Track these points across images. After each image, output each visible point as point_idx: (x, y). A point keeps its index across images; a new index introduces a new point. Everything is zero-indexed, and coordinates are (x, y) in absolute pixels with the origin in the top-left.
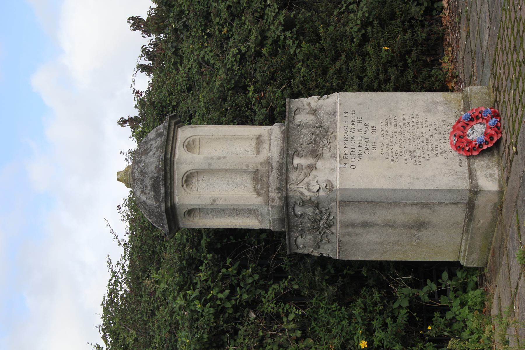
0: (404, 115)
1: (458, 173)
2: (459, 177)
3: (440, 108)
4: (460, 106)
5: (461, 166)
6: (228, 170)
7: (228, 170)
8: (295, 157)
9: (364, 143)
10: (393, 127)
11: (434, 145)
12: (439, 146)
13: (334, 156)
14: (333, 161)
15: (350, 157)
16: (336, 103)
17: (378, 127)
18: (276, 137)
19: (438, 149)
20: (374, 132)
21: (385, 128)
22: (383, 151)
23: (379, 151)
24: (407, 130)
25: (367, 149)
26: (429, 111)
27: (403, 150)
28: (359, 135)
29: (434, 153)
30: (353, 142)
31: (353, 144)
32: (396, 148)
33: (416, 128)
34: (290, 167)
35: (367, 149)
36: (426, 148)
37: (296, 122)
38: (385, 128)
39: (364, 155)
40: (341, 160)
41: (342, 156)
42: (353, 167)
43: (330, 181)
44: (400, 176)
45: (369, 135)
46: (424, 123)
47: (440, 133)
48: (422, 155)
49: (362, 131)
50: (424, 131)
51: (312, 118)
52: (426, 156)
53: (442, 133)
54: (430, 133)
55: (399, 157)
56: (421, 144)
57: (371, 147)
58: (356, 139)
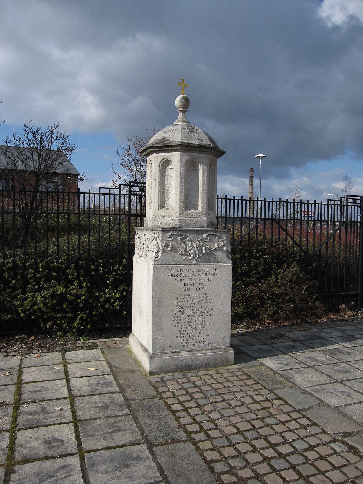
6: (235, 331)
7: (235, 331)
42: (170, 275)
47: (196, 333)
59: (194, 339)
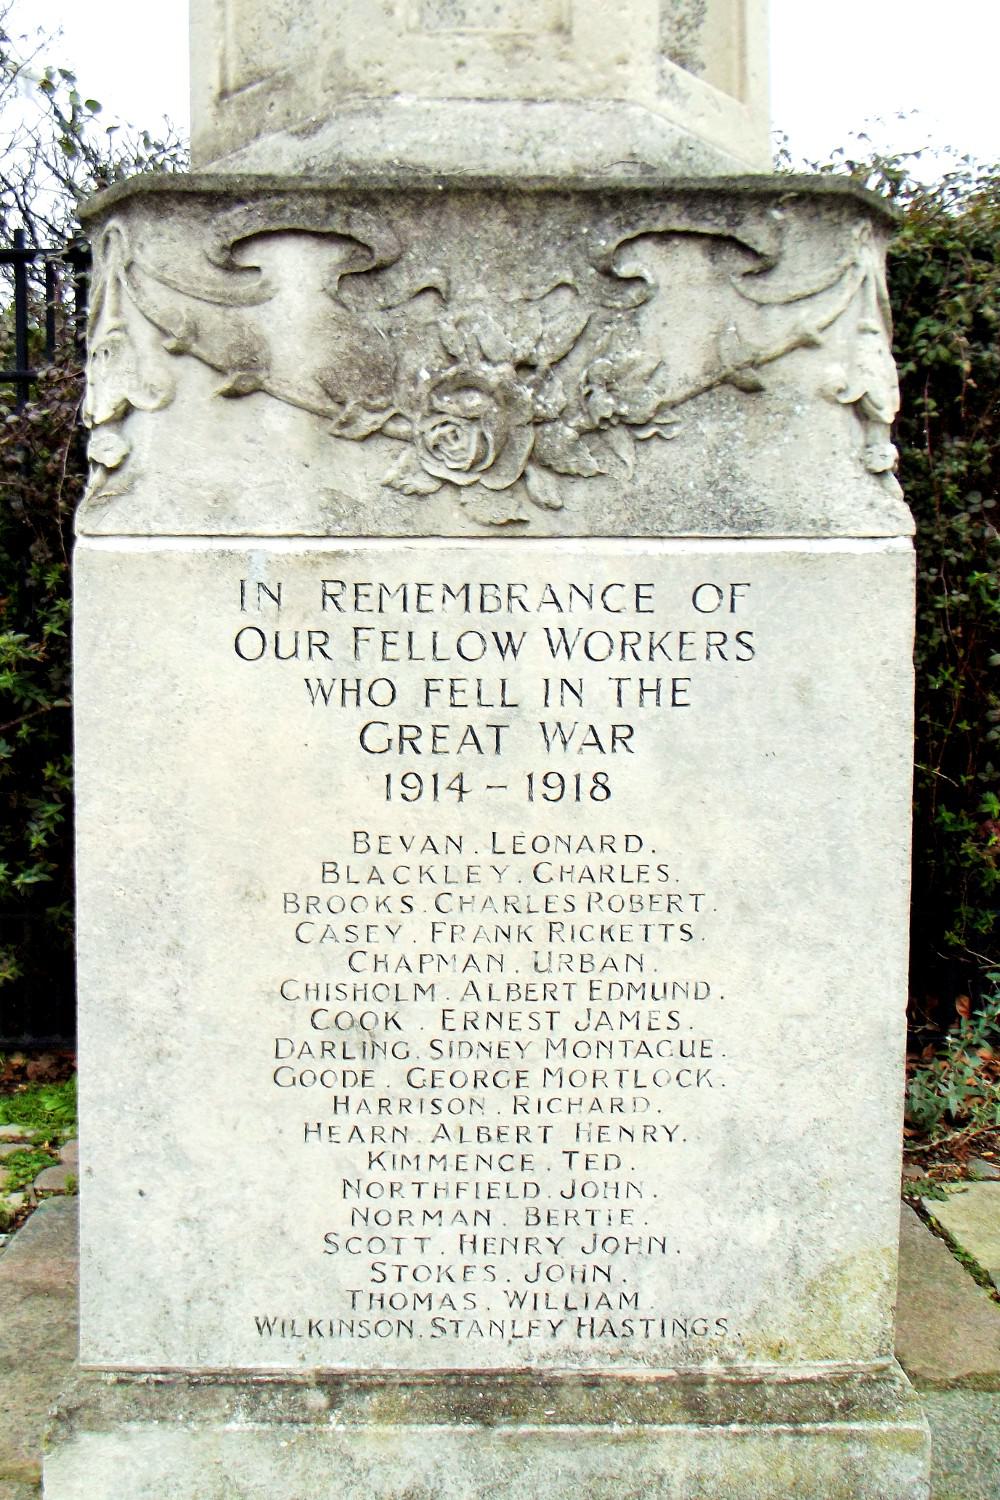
0: (701, 992)
1: (204, 1306)
2: (178, 1311)
3: (762, 1229)
4: (778, 1351)
5: (263, 1326)
8: (333, 255)
9: (461, 719)
10: (601, 916)
11: (436, 1175)
12: (427, 1201)
13: (341, 519)
14: (301, 507)
15: (340, 624)
16: (823, 529)
17: (599, 819)
18: (548, 137)
19: (407, 1199)
20: (554, 787)
21: (595, 860)
22: (393, 844)
23: (391, 817)
24: (570, 1011)
25: (406, 740)
26: (731, 1157)
27: (406, 980)
28: (525, 689)
29: (383, 1176)
30: (471, 646)
31: (447, 646)
32: (415, 927)
33: (589, 1065)
34: (239, 220)
35: (406, 740)
36: (421, 1124)
37: (647, 251)
38: (595, 860)
39: (356, 716)
40: (313, 562)
41: (348, 572)
43: (128, 490)
44: (174, 949)
45: (526, 753)
46: (633, 1120)
48: (356, 1094)
49: (566, 711)
50: (561, 1121)
51: (686, 366)
52: (344, 1122)
53: (541, 1232)
54: (536, 1149)
55: (342, 950)
56: (445, 1093)
57: (425, 765)
58: (492, 667)
59: (514, 1265)
